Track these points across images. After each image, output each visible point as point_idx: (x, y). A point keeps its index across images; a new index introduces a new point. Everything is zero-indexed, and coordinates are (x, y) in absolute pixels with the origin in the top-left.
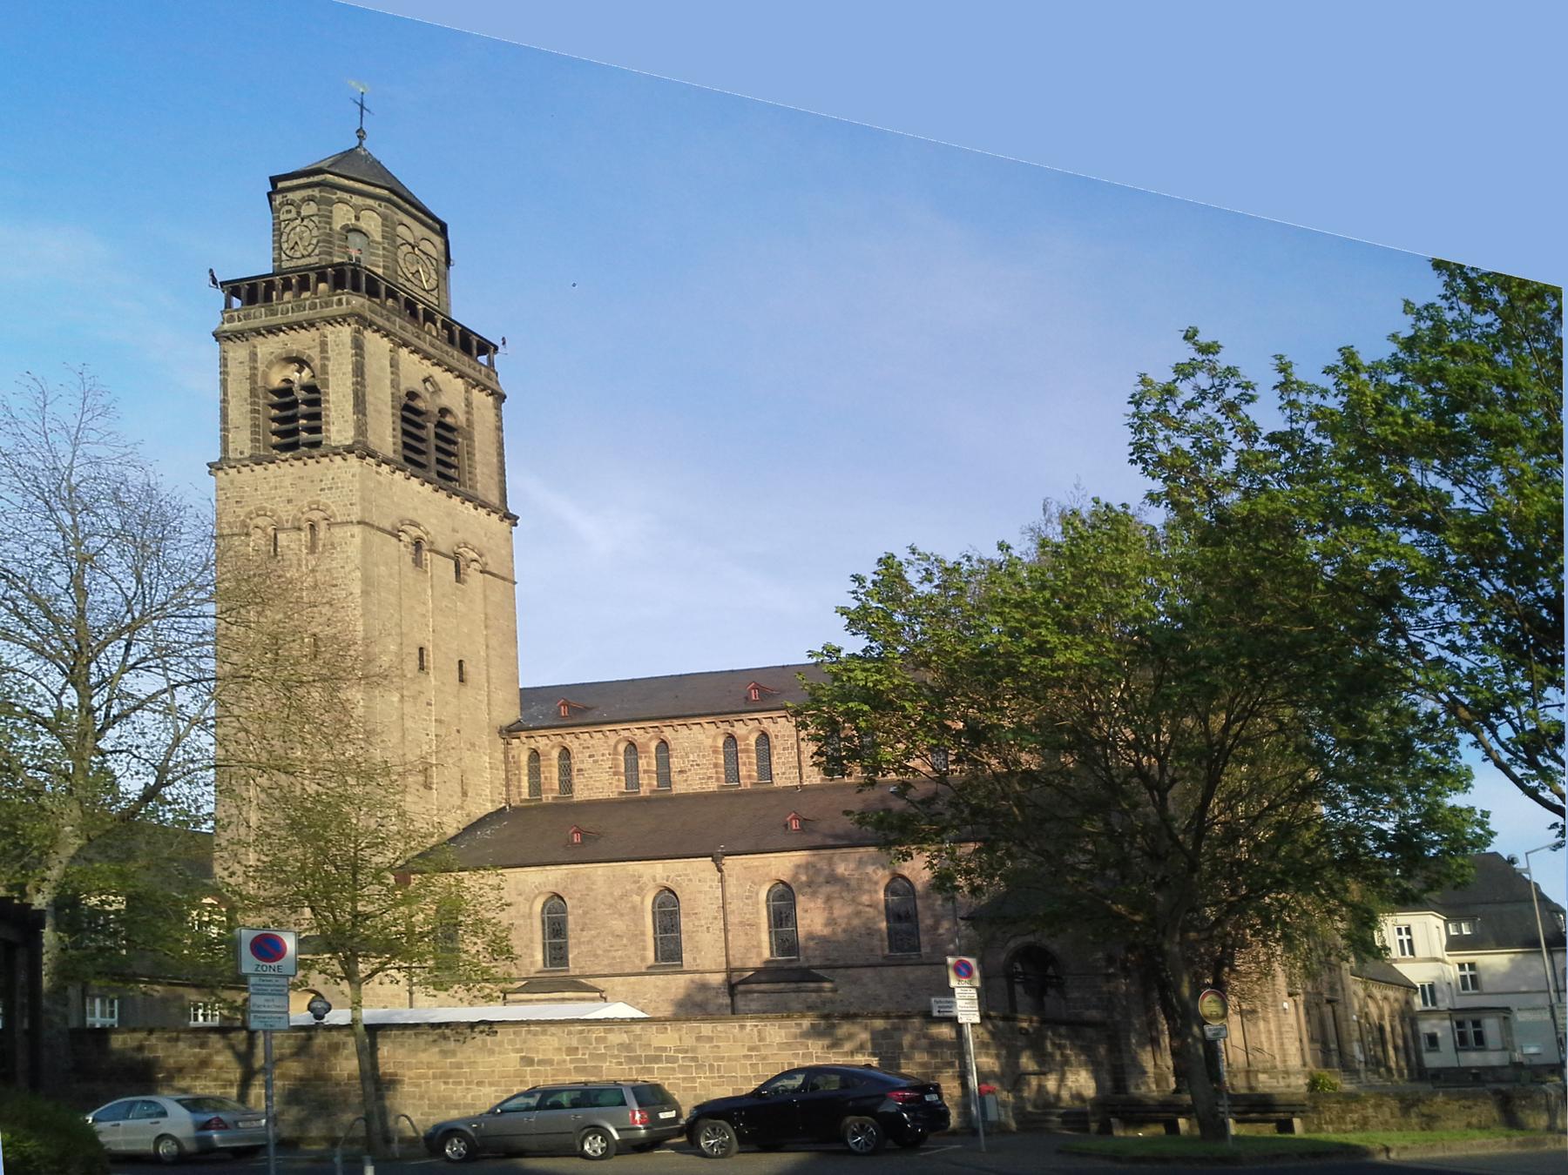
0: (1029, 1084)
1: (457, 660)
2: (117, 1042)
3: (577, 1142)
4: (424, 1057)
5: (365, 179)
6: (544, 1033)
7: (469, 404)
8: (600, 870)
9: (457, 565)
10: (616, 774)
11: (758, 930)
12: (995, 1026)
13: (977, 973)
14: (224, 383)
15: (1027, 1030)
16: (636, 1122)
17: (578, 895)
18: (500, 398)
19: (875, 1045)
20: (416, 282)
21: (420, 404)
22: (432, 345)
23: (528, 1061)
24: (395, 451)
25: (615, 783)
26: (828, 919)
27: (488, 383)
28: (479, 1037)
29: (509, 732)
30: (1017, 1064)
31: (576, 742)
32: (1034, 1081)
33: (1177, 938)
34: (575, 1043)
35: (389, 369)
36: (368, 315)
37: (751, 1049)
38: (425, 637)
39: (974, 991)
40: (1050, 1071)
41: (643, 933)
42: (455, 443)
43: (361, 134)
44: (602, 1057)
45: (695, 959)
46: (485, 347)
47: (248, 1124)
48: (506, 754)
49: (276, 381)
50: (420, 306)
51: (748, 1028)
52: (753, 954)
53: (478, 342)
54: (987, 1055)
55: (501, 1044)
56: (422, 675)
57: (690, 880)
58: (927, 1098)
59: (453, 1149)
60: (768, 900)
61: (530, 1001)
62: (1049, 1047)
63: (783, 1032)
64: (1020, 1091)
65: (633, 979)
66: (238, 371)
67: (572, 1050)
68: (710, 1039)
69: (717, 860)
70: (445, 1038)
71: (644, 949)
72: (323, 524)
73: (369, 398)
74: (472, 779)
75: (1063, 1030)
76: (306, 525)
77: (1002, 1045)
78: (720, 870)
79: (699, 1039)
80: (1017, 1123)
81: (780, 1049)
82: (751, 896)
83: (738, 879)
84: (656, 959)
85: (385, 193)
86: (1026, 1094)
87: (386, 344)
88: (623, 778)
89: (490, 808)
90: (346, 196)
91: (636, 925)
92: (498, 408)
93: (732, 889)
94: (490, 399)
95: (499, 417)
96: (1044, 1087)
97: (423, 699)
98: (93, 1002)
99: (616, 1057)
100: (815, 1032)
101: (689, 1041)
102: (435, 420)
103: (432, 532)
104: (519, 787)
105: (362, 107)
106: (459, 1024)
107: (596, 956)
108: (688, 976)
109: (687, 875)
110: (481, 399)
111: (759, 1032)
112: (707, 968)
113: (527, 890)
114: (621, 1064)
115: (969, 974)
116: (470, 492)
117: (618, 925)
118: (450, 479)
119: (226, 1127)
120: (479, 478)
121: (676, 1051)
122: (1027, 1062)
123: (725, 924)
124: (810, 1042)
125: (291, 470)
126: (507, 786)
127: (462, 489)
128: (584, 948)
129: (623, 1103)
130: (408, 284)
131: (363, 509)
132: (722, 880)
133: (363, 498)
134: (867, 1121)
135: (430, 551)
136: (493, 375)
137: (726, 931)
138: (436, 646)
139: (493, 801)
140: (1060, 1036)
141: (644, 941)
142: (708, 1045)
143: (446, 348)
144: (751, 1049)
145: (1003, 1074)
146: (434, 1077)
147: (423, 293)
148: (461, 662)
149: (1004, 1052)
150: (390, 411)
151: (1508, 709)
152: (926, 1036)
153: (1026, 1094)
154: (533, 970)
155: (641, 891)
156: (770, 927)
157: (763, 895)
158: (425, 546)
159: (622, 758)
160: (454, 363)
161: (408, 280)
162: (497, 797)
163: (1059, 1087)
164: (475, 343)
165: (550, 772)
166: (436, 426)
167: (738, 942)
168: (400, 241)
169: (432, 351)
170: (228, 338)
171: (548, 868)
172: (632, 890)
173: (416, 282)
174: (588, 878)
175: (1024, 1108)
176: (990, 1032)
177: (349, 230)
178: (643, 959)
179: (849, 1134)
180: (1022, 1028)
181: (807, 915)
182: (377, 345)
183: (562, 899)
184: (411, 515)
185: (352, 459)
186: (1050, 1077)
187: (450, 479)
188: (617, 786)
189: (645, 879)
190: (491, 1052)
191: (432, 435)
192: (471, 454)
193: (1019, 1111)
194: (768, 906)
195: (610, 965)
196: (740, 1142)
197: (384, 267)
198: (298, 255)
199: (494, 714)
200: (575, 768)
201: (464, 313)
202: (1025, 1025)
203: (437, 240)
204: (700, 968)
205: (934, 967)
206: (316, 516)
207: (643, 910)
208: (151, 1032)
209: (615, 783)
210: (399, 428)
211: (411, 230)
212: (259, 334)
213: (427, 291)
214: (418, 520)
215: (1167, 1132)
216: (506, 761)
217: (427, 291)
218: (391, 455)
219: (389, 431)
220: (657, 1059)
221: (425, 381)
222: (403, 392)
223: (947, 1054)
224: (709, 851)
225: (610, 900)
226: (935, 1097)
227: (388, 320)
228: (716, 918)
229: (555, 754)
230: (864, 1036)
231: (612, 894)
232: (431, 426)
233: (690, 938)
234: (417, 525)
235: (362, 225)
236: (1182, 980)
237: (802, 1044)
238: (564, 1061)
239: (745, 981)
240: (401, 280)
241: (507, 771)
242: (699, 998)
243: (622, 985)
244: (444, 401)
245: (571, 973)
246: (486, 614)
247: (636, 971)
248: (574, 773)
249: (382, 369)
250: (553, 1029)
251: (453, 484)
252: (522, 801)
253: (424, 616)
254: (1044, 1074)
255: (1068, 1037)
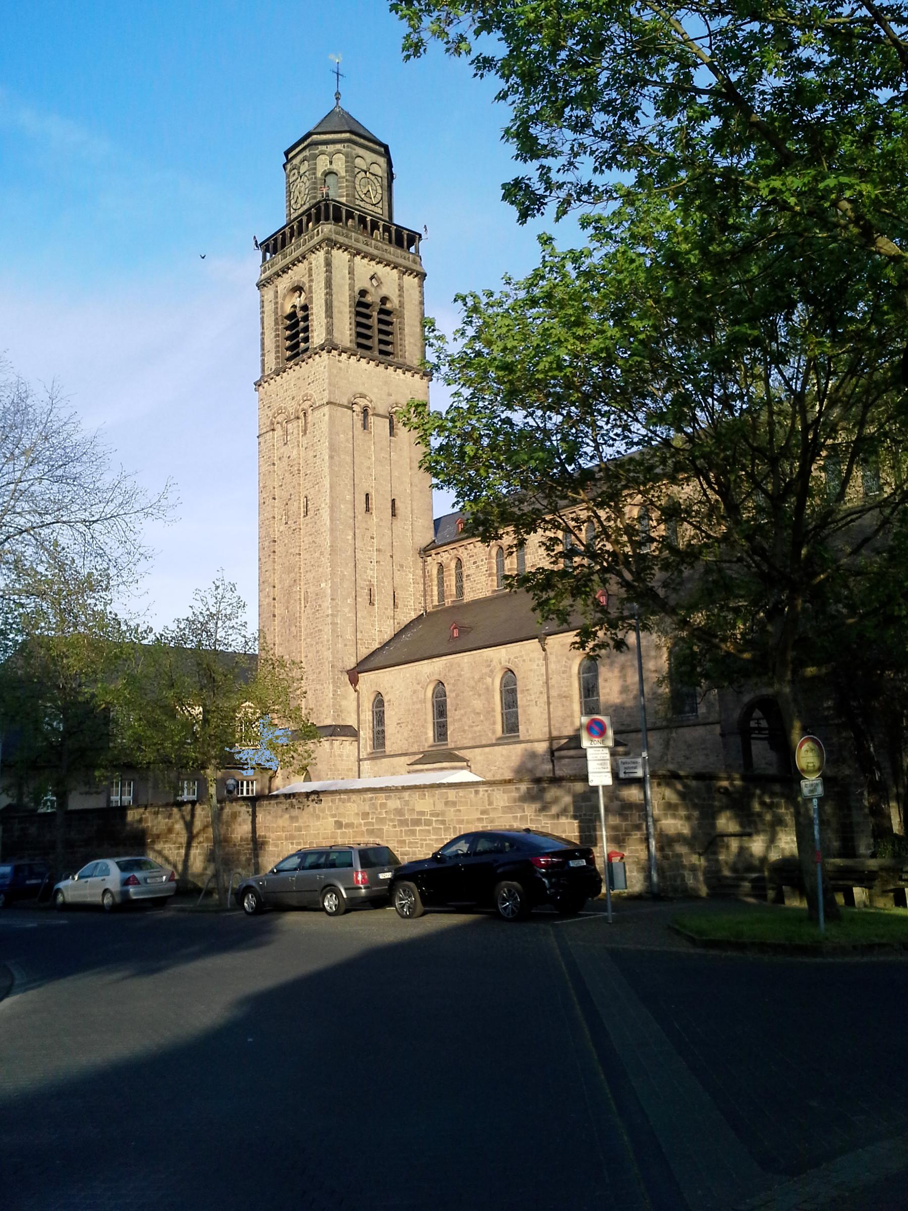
0: (728, 847)
1: (390, 500)
2: (132, 816)
3: (321, 899)
4: (281, 822)
5: (336, 129)
6: (349, 800)
7: (401, 288)
8: (465, 659)
9: (391, 422)
10: (490, 575)
11: (571, 701)
12: (685, 786)
13: (610, 733)
14: (263, 323)
15: (726, 789)
16: (358, 881)
17: (453, 681)
18: (422, 276)
19: (577, 808)
20: (368, 200)
21: (369, 299)
22: (376, 248)
23: (339, 825)
24: (351, 341)
25: (490, 583)
26: (623, 686)
27: (415, 267)
28: (312, 805)
29: (425, 552)
30: (713, 826)
31: (466, 552)
32: (734, 844)
33: (789, 676)
34: (367, 809)
35: (348, 276)
36: (334, 237)
37: (483, 812)
38: (366, 485)
39: (607, 751)
40: (758, 832)
41: (493, 710)
42: (391, 323)
43: (338, 96)
44: (381, 821)
45: (527, 731)
46: (413, 238)
47: (153, 880)
48: (424, 569)
49: (288, 310)
50: (369, 218)
51: (481, 793)
52: (568, 724)
53: (408, 235)
54: (674, 816)
55: (323, 811)
56: (368, 515)
57: (524, 661)
58: (572, 864)
59: (249, 903)
60: (579, 673)
61: (422, 771)
62: (757, 807)
63: (506, 796)
64: (715, 853)
65: (487, 749)
66: (269, 307)
67: (365, 815)
68: (454, 804)
69: (542, 641)
70: (292, 806)
71: (494, 723)
72: (310, 411)
73: (335, 303)
74: (400, 594)
75: (777, 788)
76: (301, 414)
77: (695, 806)
78: (544, 650)
79: (447, 803)
80: (709, 887)
81: (504, 812)
82: (567, 670)
83: (557, 657)
84: (503, 732)
85: (347, 135)
86: (722, 857)
87: (346, 256)
88: (495, 578)
89: (413, 616)
90: (323, 148)
91: (489, 702)
92: (421, 286)
93: (552, 666)
94: (416, 279)
95: (422, 293)
96: (748, 849)
97: (369, 534)
98: (183, 783)
99: (392, 820)
100: (530, 797)
101: (440, 807)
102: (377, 308)
103: (374, 400)
104: (432, 596)
105: (338, 74)
106: (300, 794)
107: (464, 731)
108: (523, 745)
109: (521, 656)
110: (410, 281)
111: (489, 796)
112: (536, 737)
113: (423, 679)
114: (395, 826)
115: (602, 733)
116: (401, 360)
117: (478, 704)
118: (387, 354)
119: (139, 883)
120: (407, 348)
121: (432, 815)
122: (726, 823)
123: (548, 697)
124: (526, 806)
125: (294, 374)
126: (425, 596)
127: (396, 360)
128: (457, 725)
129: (351, 865)
130: (362, 204)
131: (330, 393)
132: (546, 659)
133: (330, 384)
134: (513, 887)
135: (373, 415)
136: (418, 259)
137: (549, 703)
138: (377, 490)
139: (415, 610)
140: (772, 795)
141: (494, 716)
142: (452, 809)
143: (385, 247)
144: (483, 812)
145: (694, 836)
146: (286, 839)
147: (372, 208)
148: (393, 500)
149: (696, 814)
150: (347, 309)
151: (606, 145)
152: (617, 798)
153: (722, 857)
154: (427, 745)
155: (491, 673)
156: (581, 698)
157: (575, 669)
158: (370, 412)
159: (494, 561)
160: (391, 258)
161: (363, 200)
162: (419, 606)
163: (768, 848)
164: (405, 236)
165: (450, 580)
166: (379, 313)
167: (558, 712)
168: (357, 170)
169: (375, 252)
170: (264, 285)
171: (434, 660)
172: (486, 673)
173: (368, 200)
174: (459, 666)
175: (720, 871)
176: (679, 793)
177: (328, 173)
178: (494, 732)
179: (499, 902)
180: (721, 787)
181: (607, 684)
182: (340, 257)
183: (443, 684)
184: (361, 389)
185: (324, 354)
186: (755, 838)
187: (387, 354)
188: (491, 586)
189: (494, 663)
190: (318, 817)
191: (376, 321)
192: (402, 329)
193: (713, 876)
194: (579, 678)
195: (473, 738)
196: (424, 903)
197: (347, 195)
198: (299, 206)
199: (416, 538)
200: (465, 574)
201: (402, 218)
202: (725, 783)
203: (382, 161)
204: (531, 738)
205: (708, 727)
206: (306, 405)
207: (493, 691)
208: (146, 807)
209: (490, 583)
210: (353, 321)
211: (367, 158)
212: (279, 276)
213: (374, 205)
214: (365, 392)
215: (846, 902)
216: (424, 577)
217: (374, 205)
218: (348, 345)
219: (347, 327)
220: (417, 822)
221: (372, 278)
222: (357, 290)
223: (635, 818)
224: (535, 633)
225: (472, 683)
226: (583, 863)
227: (347, 236)
228: (541, 693)
229: (453, 565)
230: (567, 799)
231: (473, 678)
232: (375, 314)
233: (525, 711)
234: (363, 396)
235: (334, 167)
236: (792, 727)
237: (520, 807)
238: (361, 825)
239: (560, 749)
240: (358, 202)
241: (425, 584)
242: (530, 765)
243: (481, 755)
244: (384, 291)
245: (449, 747)
246: (410, 459)
247: (489, 742)
248: (464, 579)
249: (343, 278)
250: (354, 797)
251: (390, 358)
252: (434, 607)
253: (369, 468)
254: (750, 835)
255: (782, 795)
